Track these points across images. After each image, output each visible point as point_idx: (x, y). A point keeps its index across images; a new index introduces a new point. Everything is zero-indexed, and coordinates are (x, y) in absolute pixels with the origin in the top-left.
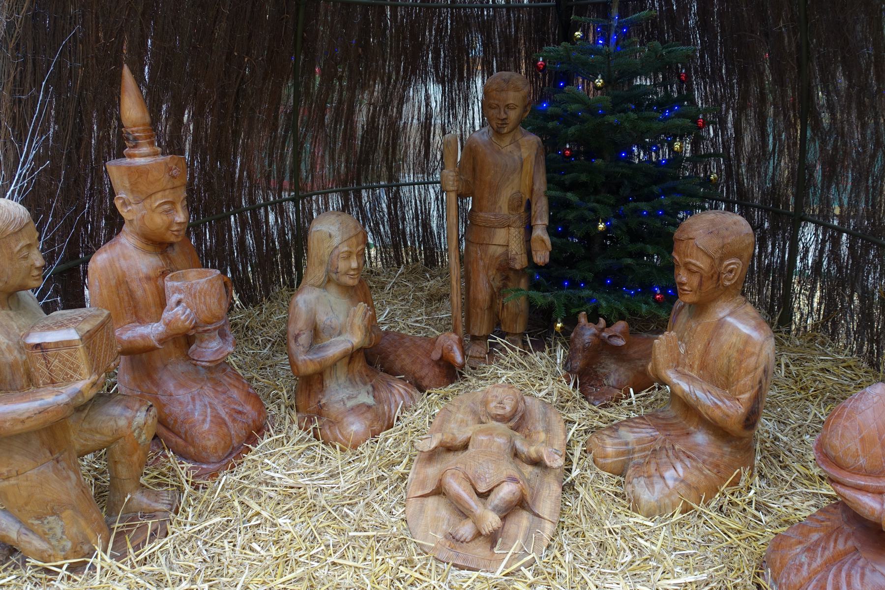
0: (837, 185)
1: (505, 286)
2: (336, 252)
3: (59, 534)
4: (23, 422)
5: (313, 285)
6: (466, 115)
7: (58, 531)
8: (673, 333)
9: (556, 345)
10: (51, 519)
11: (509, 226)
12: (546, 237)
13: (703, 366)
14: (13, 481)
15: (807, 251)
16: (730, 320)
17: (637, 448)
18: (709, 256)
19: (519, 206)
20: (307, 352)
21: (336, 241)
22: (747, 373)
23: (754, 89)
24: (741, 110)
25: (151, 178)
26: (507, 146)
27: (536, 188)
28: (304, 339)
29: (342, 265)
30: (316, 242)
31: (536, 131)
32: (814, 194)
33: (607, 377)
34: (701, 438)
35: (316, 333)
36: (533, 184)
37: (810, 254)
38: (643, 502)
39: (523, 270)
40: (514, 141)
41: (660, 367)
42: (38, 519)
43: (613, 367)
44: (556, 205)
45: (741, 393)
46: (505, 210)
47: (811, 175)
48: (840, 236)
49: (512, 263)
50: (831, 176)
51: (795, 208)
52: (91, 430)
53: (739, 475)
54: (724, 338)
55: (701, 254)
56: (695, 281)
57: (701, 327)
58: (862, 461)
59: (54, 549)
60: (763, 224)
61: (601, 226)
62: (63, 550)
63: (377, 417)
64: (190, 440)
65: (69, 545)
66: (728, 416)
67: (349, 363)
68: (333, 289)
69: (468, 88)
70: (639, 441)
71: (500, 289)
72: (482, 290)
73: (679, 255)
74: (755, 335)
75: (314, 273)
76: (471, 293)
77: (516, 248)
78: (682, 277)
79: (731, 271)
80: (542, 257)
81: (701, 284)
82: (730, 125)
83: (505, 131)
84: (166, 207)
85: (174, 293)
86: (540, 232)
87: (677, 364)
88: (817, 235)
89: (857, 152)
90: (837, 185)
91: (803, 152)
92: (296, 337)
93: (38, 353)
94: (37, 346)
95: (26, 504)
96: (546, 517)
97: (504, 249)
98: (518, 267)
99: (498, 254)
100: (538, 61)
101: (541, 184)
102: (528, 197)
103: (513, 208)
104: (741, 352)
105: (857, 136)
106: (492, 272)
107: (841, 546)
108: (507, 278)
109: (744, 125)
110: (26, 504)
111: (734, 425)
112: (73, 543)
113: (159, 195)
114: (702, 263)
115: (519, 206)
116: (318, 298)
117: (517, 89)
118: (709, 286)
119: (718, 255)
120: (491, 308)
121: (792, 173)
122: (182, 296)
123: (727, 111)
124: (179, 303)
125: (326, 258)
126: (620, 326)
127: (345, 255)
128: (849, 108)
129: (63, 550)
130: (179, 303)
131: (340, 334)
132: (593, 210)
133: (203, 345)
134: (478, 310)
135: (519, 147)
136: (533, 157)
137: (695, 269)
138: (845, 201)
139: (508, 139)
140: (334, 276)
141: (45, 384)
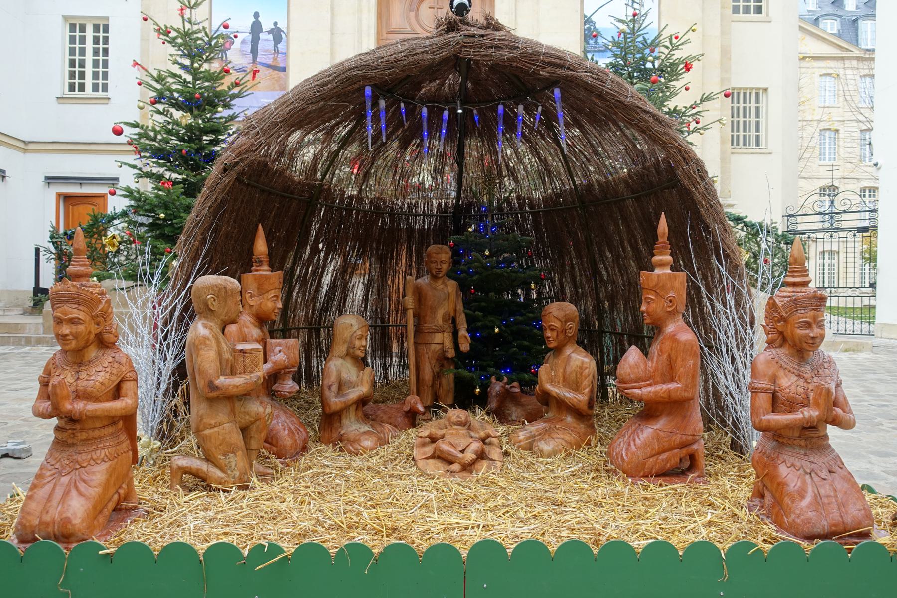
0: (617, 310)
1: (441, 370)
2: (355, 335)
3: (233, 467)
4: (237, 387)
5: (338, 357)
6: (393, 281)
7: (233, 464)
8: (547, 365)
9: (475, 408)
10: (231, 455)
11: (443, 332)
12: (467, 335)
13: (565, 380)
14: (216, 429)
15: (609, 352)
16: (573, 355)
17: (537, 433)
18: (560, 320)
19: (449, 319)
20: (336, 397)
21: (355, 328)
22: (585, 378)
23: (567, 261)
24: (562, 274)
25: (271, 281)
26: (439, 285)
27: (458, 309)
28: (335, 388)
29: (358, 343)
30: (341, 331)
31: (454, 279)
32: (607, 317)
33: (510, 415)
34: (569, 419)
35: (342, 385)
36: (456, 307)
37: (611, 353)
38: (545, 451)
39: (452, 359)
40: (444, 283)
41: (543, 383)
42: (224, 455)
43: (514, 408)
44: (470, 320)
45: (584, 389)
46: (440, 322)
47: (604, 307)
48: (623, 337)
49: (446, 354)
50: (613, 307)
51: (599, 328)
52: (245, 412)
53: (590, 440)
54: (572, 363)
55: (556, 320)
56: (555, 334)
57: (560, 361)
58: (632, 376)
59: (229, 477)
60: (583, 341)
61: (497, 330)
62: (234, 478)
63: (379, 438)
64: (274, 442)
65: (237, 474)
66: (580, 401)
67: (356, 409)
68: (349, 360)
69: (396, 264)
70: (537, 430)
71: (438, 373)
72: (427, 373)
73: (545, 323)
74: (586, 360)
75: (340, 349)
76: (420, 376)
77: (448, 344)
78: (549, 334)
79: (570, 329)
80: (465, 347)
81: (557, 336)
82: (557, 283)
83: (440, 275)
84: (275, 298)
85: (276, 346)
86: (463, 332)
87: (551, 381)
88: (612, 341)
89: (622, 290)
90: (617, 310)
91: (597, 294)
92: (330, 387)
93: (241, 355)
94: (241, 350)
95: (220, 444)
96: (496, 459)
97: (441, 346)
98: (450, 356)
99: (437, 349)
100: (470, 226)
101: (460, 307)
102: (452, 315)
103: (445, 320)
104: (581, 368)
105: (620, 281)
106: (433, 362)
107: (634, 428)
108: (442, 366)
109: (564, 282)
110: (220, 444)
111: (584, 407)
112: (240, 473)
113: (273, 291)
114: (557, 324)
115: (449, 319)
116: (342, 364)
117: (446, 253)
118: (561, 337)
119: (563, 320)
120: (432, 386)
121: (594, 307)
122: (280, 348)
123: (554, 275)
124: (280, 351)
125: (348, 339)
126: (515, 384)
127: (359, 337)
128: (614, 267)
129: (234, 478)
130: (280, 351)
131: (354, 387)
132: (492, 321)
133: (285, 383)
134: (426, 387)
135: (446, 285)
136: (455, 292)
137: (554, 328)
138: (622, 318)
139: (440, 281)
140: (351, 351)
141: (240, 373)
